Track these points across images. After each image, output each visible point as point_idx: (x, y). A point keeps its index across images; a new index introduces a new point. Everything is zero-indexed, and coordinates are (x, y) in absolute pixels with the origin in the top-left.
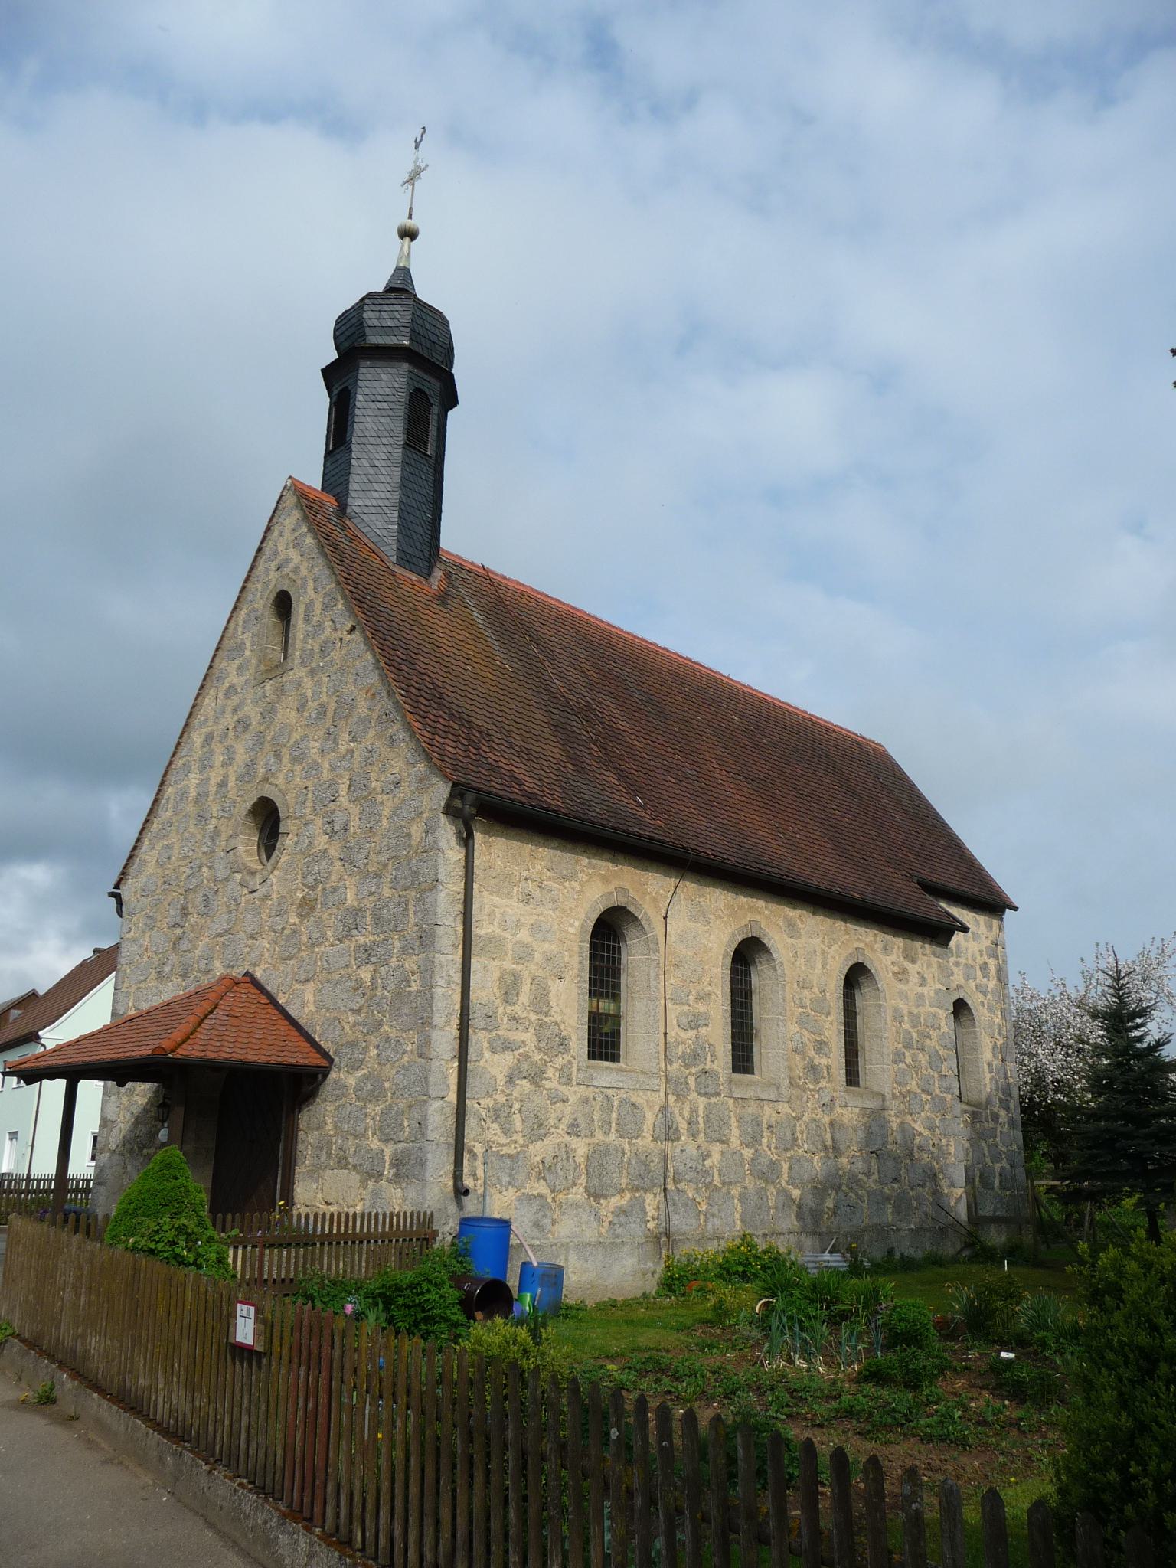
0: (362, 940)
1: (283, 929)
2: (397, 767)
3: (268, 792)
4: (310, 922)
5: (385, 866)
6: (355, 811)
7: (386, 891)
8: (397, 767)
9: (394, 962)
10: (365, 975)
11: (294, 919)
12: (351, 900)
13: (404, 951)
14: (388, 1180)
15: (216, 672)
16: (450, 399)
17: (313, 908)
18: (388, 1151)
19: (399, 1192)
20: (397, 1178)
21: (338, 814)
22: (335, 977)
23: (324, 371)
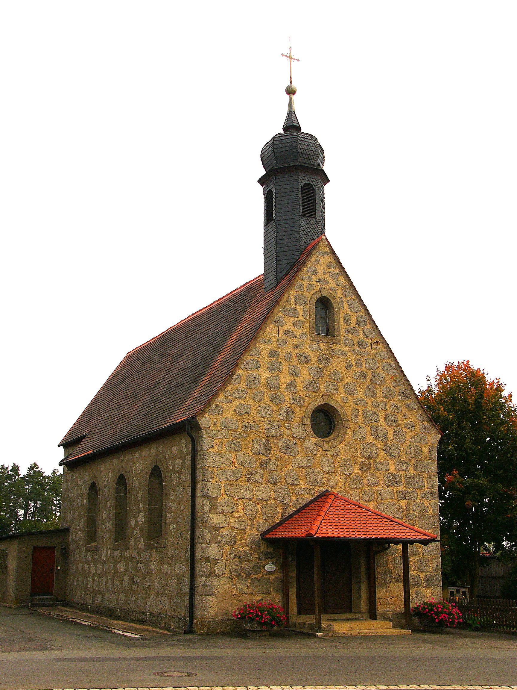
0: (400, 489)
1: (350, 474)
2: (412, 419)
3: (338, 400)
4: (367, 475)
5: (410, 460)
6: (390, 432)
7: (412, 471)
8: (412, 419)
9: (418, 501)
10: (403, 503)
11: (357, 471)
12: (392, 469)
13: (423, 497)
14: (423, 587)
15: (389, 353)
16: (323, 150)
17: (369, 469)
18: (422, 576)
19: (428, 591)
20: (428, 586)
21: (380, 428)
22: (386, 502)
23: (329, 181)
